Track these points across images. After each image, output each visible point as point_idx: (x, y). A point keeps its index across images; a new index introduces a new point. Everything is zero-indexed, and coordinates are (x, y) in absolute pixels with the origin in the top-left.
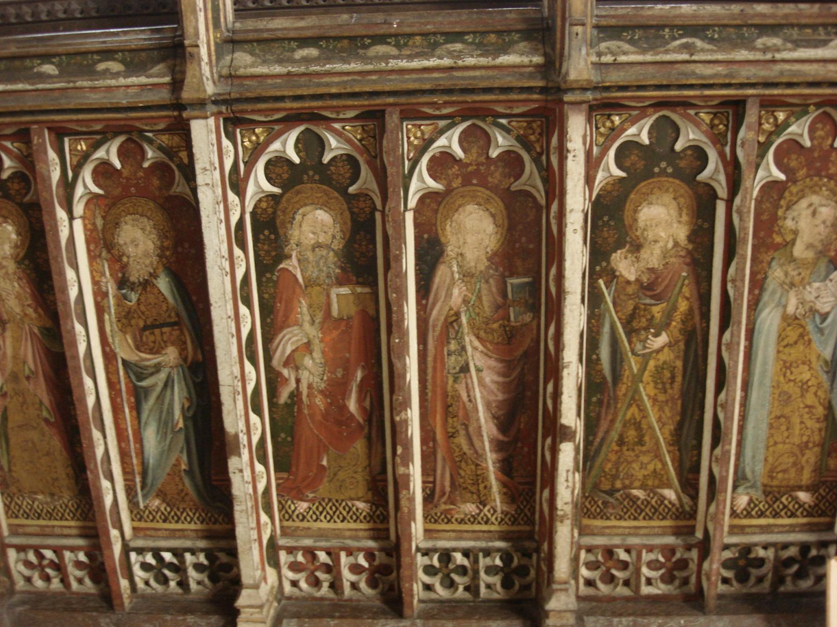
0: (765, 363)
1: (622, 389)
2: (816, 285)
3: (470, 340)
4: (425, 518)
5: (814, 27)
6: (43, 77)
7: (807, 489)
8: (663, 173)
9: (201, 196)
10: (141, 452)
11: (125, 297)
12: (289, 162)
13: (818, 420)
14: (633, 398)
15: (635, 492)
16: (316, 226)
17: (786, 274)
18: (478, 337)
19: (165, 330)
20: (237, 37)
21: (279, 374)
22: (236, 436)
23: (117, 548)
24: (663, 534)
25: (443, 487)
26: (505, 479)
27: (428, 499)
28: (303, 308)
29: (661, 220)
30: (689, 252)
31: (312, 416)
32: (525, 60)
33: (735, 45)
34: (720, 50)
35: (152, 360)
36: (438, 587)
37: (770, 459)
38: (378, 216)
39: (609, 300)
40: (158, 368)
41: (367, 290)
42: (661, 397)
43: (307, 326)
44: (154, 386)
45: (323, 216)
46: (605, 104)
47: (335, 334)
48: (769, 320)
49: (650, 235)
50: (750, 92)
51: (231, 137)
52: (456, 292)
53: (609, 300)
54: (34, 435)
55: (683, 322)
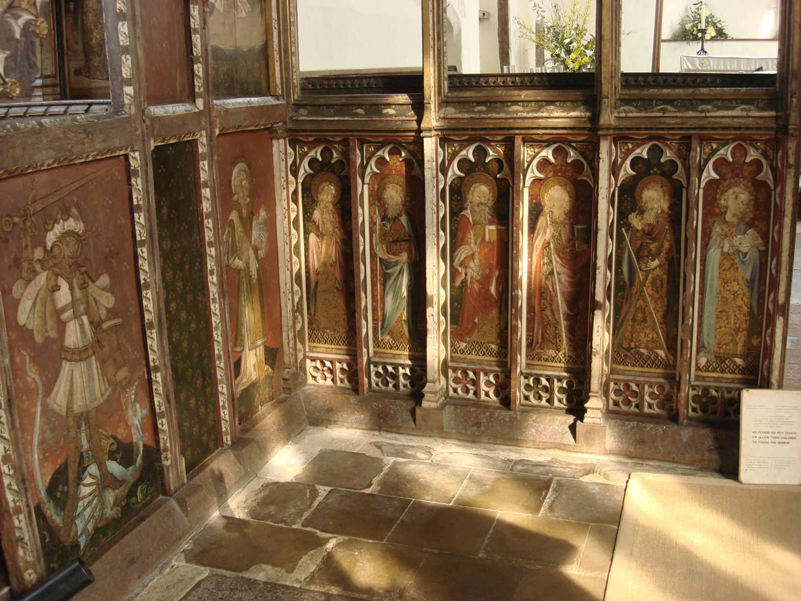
0: (712, 279)
1: (635, 289)
2: (739, 236)
4: (527, 356)
5: (730, 100)
6: (358, 115)
8: (655, 173)
9: (426, 173)
10: (383, 309)
11: (384, 225)
12: (470, 161)
13: (744, 315)
14: (640, 295)
15: (642, 350)
16: (481, 193)
17: (722, 230)
18: (559, 256)
19: (403, 243)
20: (449, 100)
21: (457, 270)
22: (432, 296)
23: (365, 359)
24: (658, 377)
25: (537, 338)
26: (570, 336)
27: (529, 345)
28: (471, 235)
29: (655, 198)
30: (669, 216)
31: (472, 294)
32: (583, 114)
33: (687, 109)
34: (680, 111)
35: (394, 259)
36: (532, 398)
37: (718, 336)
38: (511, 189)
39: (627, 239)
40: (397, 263)
41: (503, 228)
42: (656, 295)
43: (472, 245)
44: (393, 273)
45: (484, 189)
46: (621, 137)
47: (486, 250)
48: (714, 255)
49: (649, 206)
50: (692, 132)
51: (443, 148)
52: (548, 231)
53: (627, 239)
54: (330, 296)
55: (667, 254)
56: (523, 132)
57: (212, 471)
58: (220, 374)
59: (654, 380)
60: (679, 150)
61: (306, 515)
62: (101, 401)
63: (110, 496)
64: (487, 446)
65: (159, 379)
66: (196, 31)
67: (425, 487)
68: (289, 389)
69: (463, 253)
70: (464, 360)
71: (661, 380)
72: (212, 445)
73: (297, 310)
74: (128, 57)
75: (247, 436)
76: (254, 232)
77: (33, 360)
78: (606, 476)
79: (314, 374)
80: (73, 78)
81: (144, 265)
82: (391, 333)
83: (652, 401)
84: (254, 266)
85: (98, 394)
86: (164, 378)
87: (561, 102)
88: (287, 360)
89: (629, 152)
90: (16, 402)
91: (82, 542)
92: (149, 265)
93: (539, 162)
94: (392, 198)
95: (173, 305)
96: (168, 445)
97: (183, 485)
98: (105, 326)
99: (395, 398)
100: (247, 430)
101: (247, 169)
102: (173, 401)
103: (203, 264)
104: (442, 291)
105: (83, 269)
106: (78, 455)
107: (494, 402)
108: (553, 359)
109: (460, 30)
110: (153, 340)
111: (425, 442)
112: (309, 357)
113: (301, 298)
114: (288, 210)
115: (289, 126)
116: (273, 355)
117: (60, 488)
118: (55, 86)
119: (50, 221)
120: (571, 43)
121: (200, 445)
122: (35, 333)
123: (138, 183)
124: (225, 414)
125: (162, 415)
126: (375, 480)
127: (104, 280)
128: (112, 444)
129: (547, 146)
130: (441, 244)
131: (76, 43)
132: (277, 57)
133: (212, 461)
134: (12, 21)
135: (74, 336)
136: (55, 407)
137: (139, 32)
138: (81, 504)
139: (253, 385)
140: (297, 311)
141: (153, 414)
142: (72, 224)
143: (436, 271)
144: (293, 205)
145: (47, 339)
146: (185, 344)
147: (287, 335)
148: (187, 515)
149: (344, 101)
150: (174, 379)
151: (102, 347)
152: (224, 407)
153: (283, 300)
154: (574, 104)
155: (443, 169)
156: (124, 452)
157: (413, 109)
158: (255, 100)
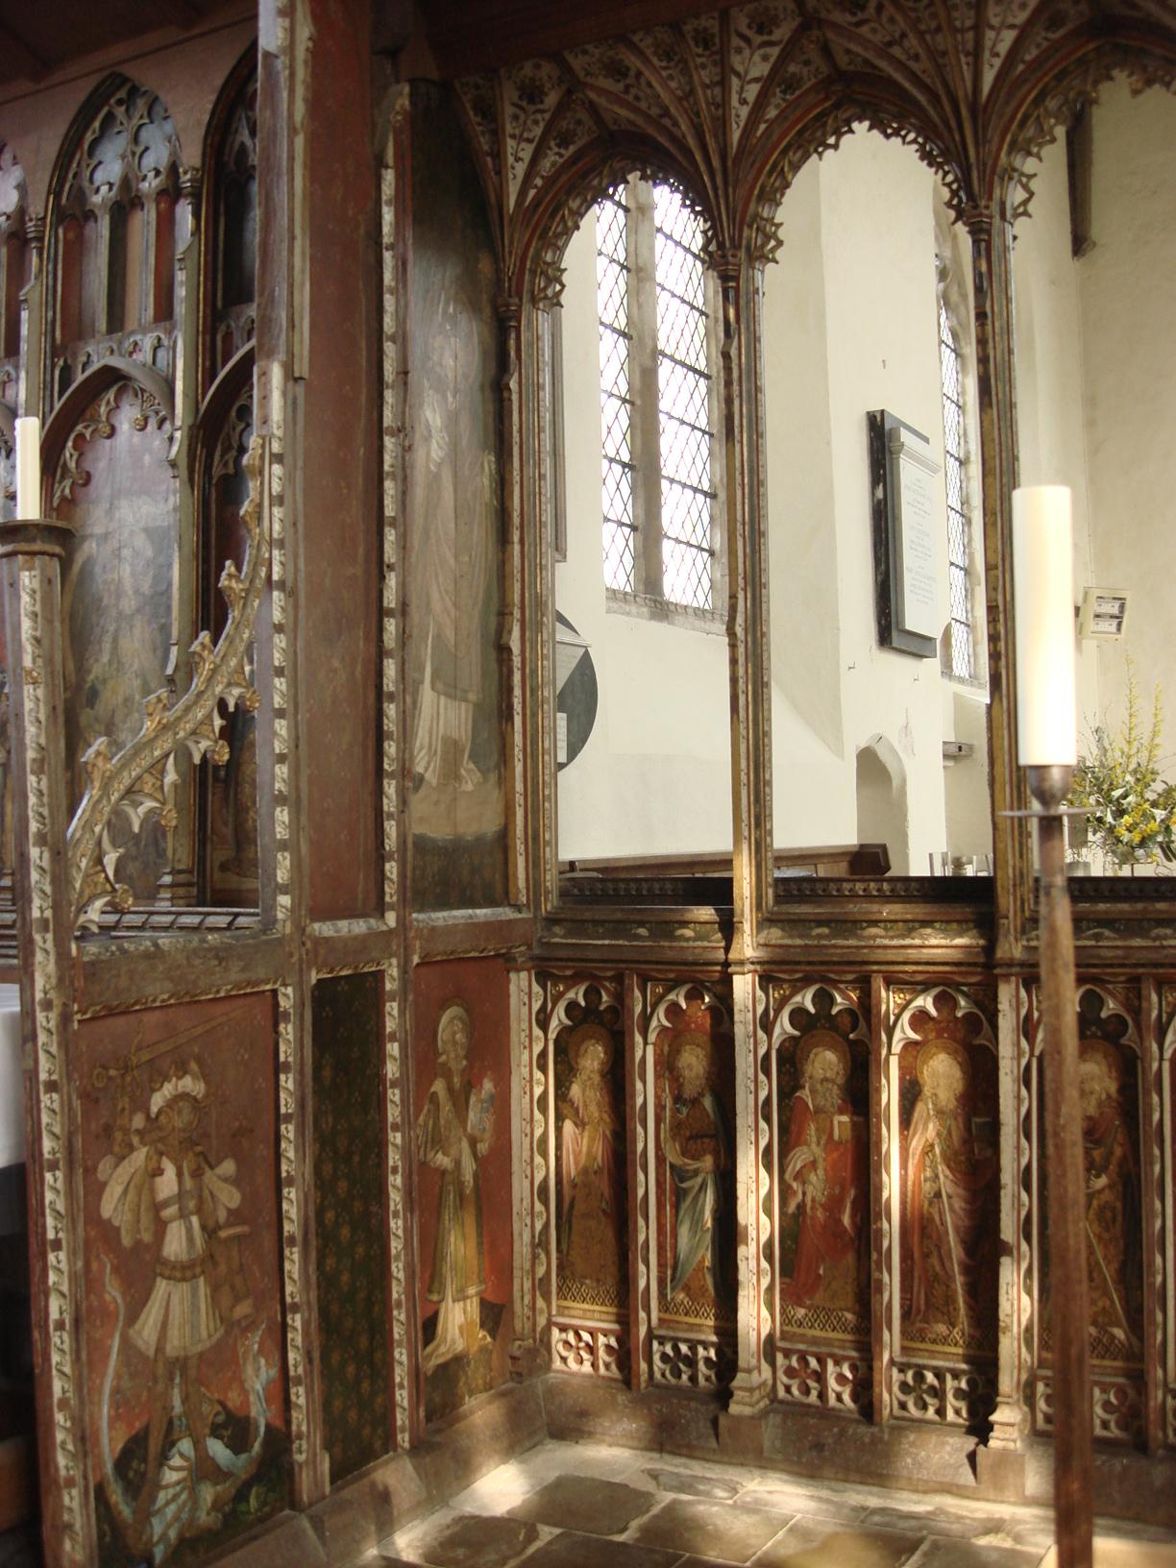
4: (904, 1333)
12: (807, 1012)
16: (826, 1063)
21: (790, 1187)
27: (906, 1316)
28: (812, 1129)
32: (974, 942)
33: (1133, 934)
34: (1121, 938)
35: (693, 1165)
36: (911, 1405)
40: (696, 1172)
42: (1106, 1236)
45: (830, 1056)
50: (1141, 970)
52: (931, 1126)
56: (883, 968)
57: (373, 1485)
58: (398, 1331)
59: (1108, 1379)
60: (1127, 998)
62: (208, 1344)
63: (208, 1493)
64: (833, 1484)
65: (298, 1324)
66: (390, 816)
67: (717, 1537)
68: (520, 1374)
69: (799, 1158)
70: (803, 1338)
71: (1121, 1380)
72: (378, 1444)
73: (540, 1243)
74: (287, 854)
75: (438, 1439)
76: (471, 1115)
77: (116, 1270)
78: (1018, 1538)
79: (564, 1353)
80: (217, 875)
81: (289, 1150)
82: (687, 1289)
83: (1106, 1417)
84: (469, 1167)
85: (204, 1334)
86: (306, 1324)
87: (946, 924)
88: (518, 1326)
90: (85, 1326)
91: (159, 1553)
92: (296, 1151)
93: (913, 1016)
94: (690, 1066)
95: (330, 1215)
96: (304, 1428)
97: (324, 1497)
98: (223, 1234)
99: (690, 1399)
100: (439, 1431)
101: (465, 1016)
102: (317, 1362)
103: (382, 1157)
104: (764, 1219)
105: (199, 1149)
106: (165, 1420)
107: (850, 1411)
108: (945, 1341)
109: (904, 780)
110: (293, 1266)
111: (732, 1474)
112: (557, 1325)
113: (547, 1225)
114: (531, 1081)
115: (537, 951)
116: (494, 1315)
117: (135, 1464)
118: (189, 884)
120: (1125, 796)
121: (357, 1446)
122: (123, 1232)
123: (288, 1031)
124: (402, 1397)
125: (298, 1381)
126: (635, 1524)
127: (228, 1167)
128: (218, 1414)
129: (923, 991)
130: (763, 1144)
131: (225, 824)
132: (520, 847)
133: (374, 1469)
134: (130, 810)
136: (140, 1343)
137: (304, 819)
138: (162, 1497)
139: (459, 1360)
140: (539, 1244)
141: (285, 1379)
142: (190, 1084)
143: (754, 1184)
144: (538, 1075)
145: (138, 1243)
146: (345, 1277)
147: (522, 1285)
148: (324, 1543)
149: (619, 916)
150: (320, 1329)
151: (215, 1264)
152: (401, 1386)
153: (516, 1227)
154: (962, 925)
155: (766, 1024)
156: (235, 1429)
157: (721, 930)
158: (482, 913)
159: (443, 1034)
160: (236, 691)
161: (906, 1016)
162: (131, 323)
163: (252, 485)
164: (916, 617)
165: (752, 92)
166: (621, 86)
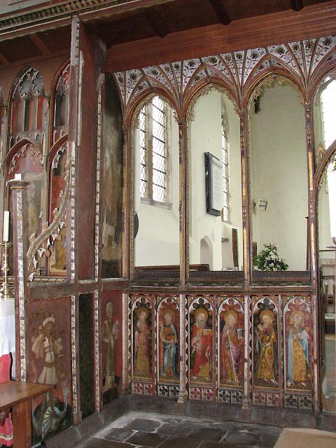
3: (230, 342)
7: (304, 382)
61: (127, 438)
63: (54, 421)
69: (195, 340)
73: (129, 361)
89: (256, 301)
91: (43, 436)
95: (82, 353)
98: (59, 356)
110: (74, 365)
113: (131, 358)
119: (45, 318)
127: (60, 340)
135: (48, 359)
142: (51, 319)
145: (40, 358)
156: (60, 405)
159: (107, 309)
160: (63, 223)
161: (222, 305)
162: (30, 129)
163: (67, 172)
164: (215, 206)
165: (188, 80)
166: (156, 77)
